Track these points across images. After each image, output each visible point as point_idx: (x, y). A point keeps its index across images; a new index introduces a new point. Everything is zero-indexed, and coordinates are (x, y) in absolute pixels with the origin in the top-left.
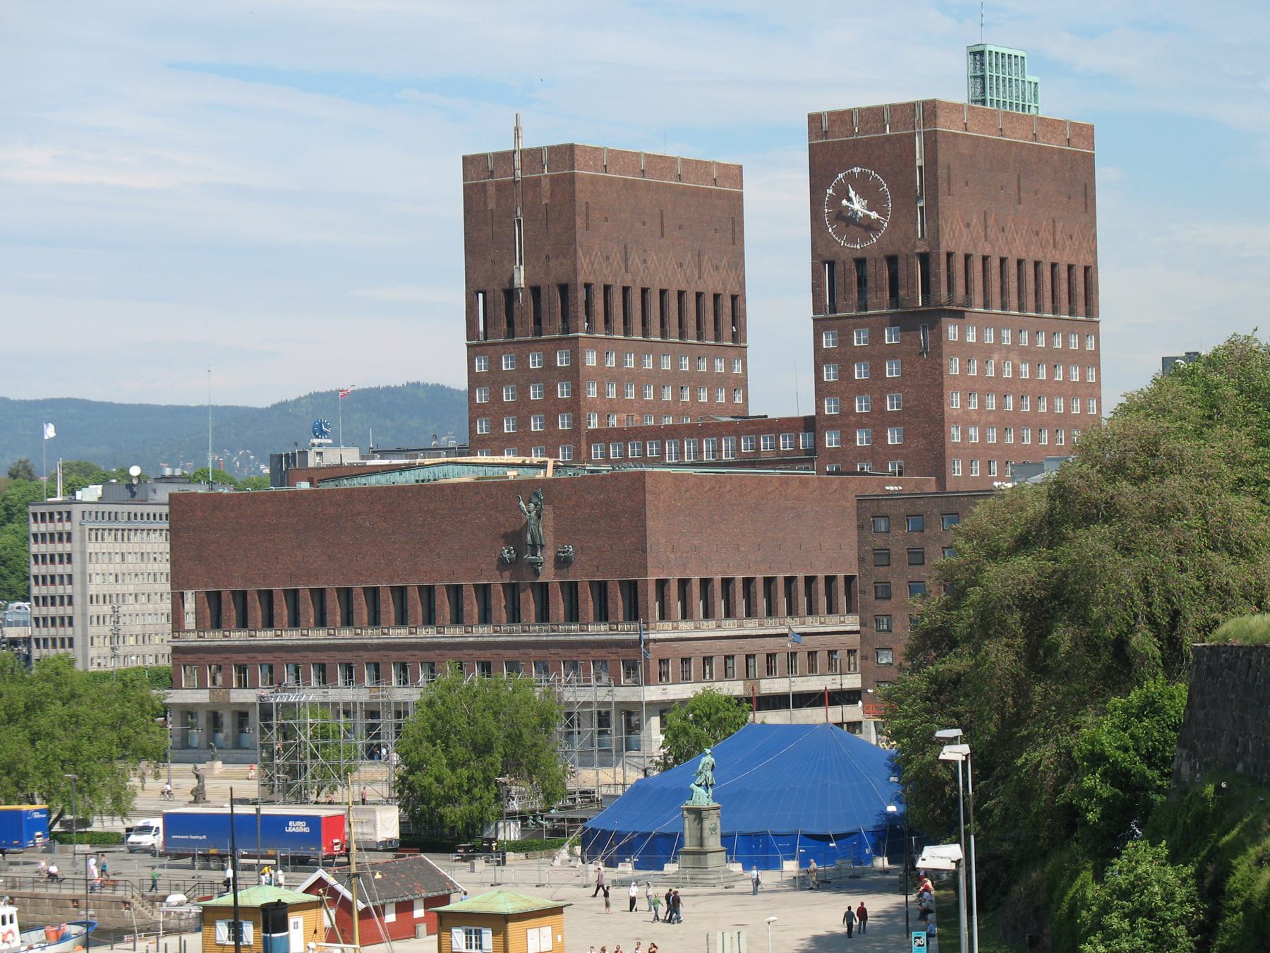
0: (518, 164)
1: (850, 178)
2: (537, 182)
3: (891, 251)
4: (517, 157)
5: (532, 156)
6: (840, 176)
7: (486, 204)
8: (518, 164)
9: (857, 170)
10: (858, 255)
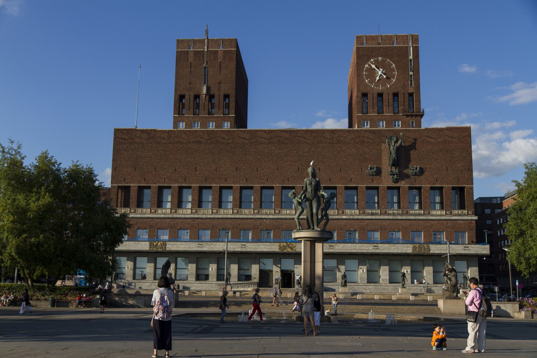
0: (206, 44)
2: (216, 52)
3: (395, 91)
4: (206, 41)
7: (188, 59)
9: (380, 58)
10: (380, 91)
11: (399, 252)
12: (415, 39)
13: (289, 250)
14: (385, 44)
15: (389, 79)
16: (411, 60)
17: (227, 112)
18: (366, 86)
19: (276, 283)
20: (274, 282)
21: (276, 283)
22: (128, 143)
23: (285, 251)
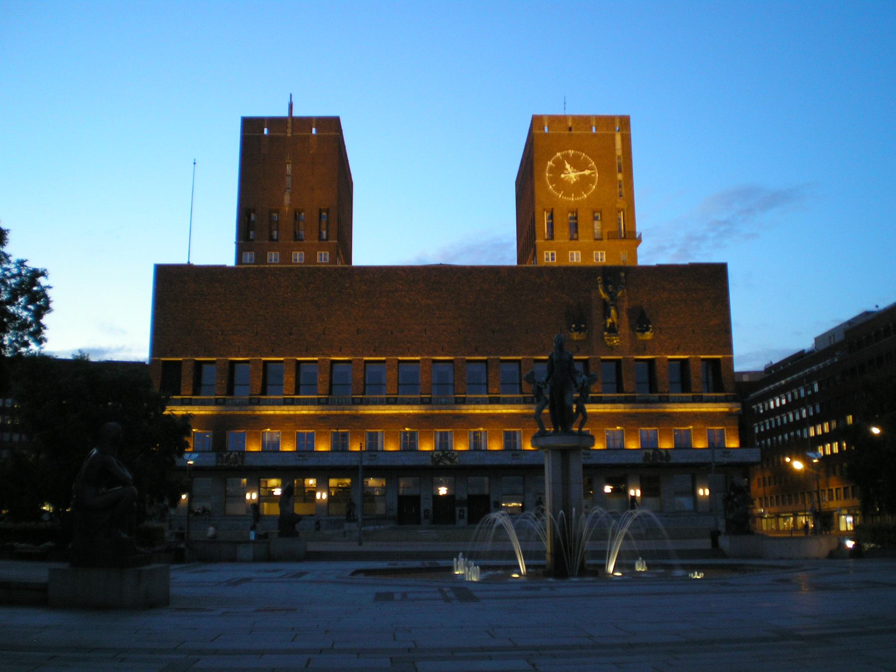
0: (289, 125)
1: (566, 157)
4: (290, 121)
5: (306, 122)
6: (558, 154)
8: (289, 125)
9: (571, 152)
11: (623, 462)
12: (625, 122)
13: (448, 463)
14: (579, 129)
15: (569, 161)
16: (619, 157)
17: (324, 237)
18: (549, 194)
19: (426, 517)
20: (422, 515)
21: (426, 517)
22: (177, 288)
23: (441, 464)
